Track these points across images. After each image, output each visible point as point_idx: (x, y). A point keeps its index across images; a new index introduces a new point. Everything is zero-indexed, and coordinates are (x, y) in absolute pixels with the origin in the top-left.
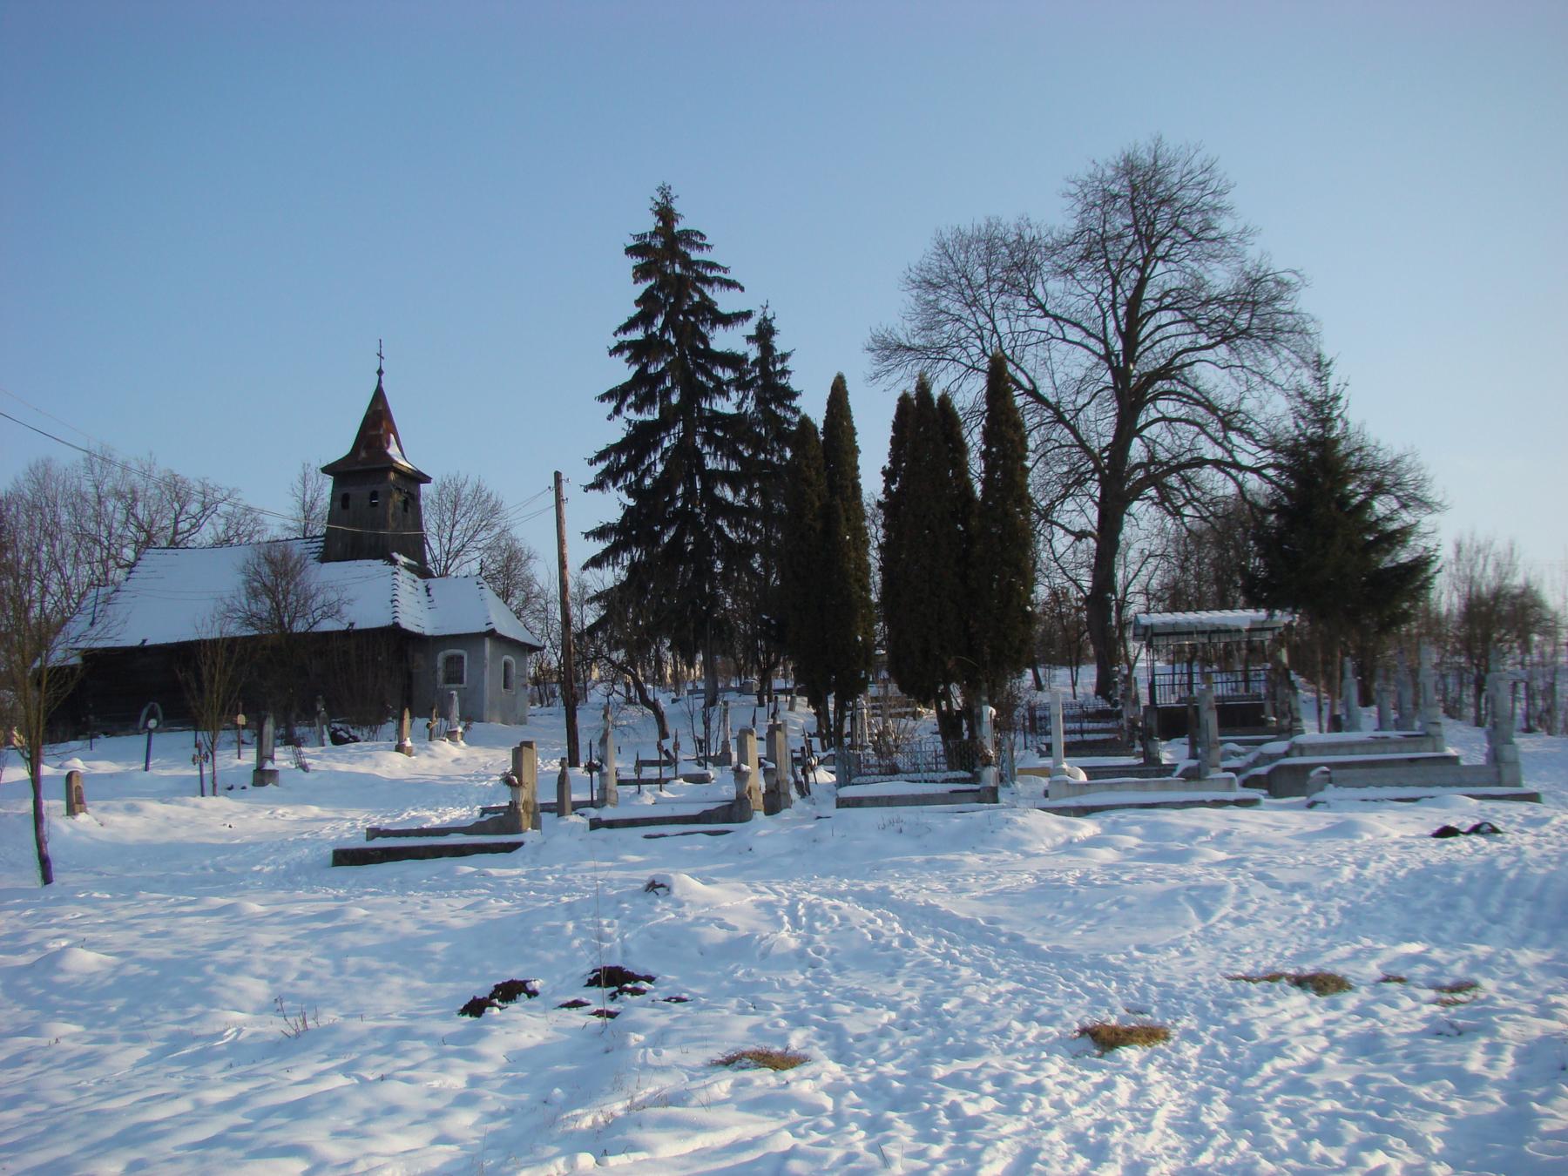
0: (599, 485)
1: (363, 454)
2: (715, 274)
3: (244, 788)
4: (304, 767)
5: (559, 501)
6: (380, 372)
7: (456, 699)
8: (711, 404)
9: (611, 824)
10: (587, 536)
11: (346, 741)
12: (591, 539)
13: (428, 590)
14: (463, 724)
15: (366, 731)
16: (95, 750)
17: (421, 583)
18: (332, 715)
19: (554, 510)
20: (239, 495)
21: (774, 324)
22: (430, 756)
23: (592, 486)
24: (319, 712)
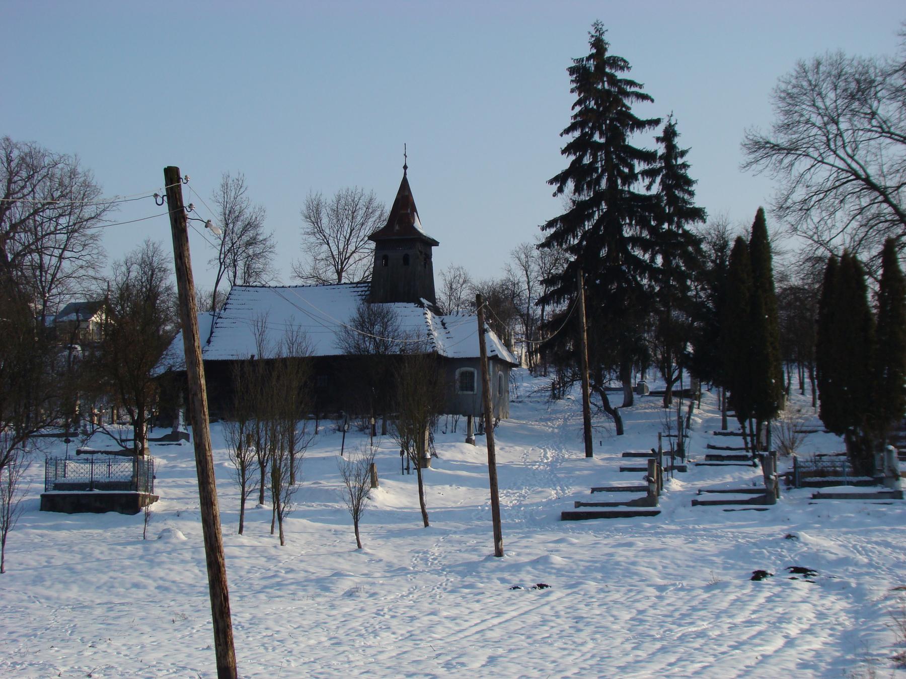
1: (397, 227)
2: (633, 89)
6: (405, 167)
8: (629, 187)
9: (703, 503)
13: (443, 324)
21: (677, 128)
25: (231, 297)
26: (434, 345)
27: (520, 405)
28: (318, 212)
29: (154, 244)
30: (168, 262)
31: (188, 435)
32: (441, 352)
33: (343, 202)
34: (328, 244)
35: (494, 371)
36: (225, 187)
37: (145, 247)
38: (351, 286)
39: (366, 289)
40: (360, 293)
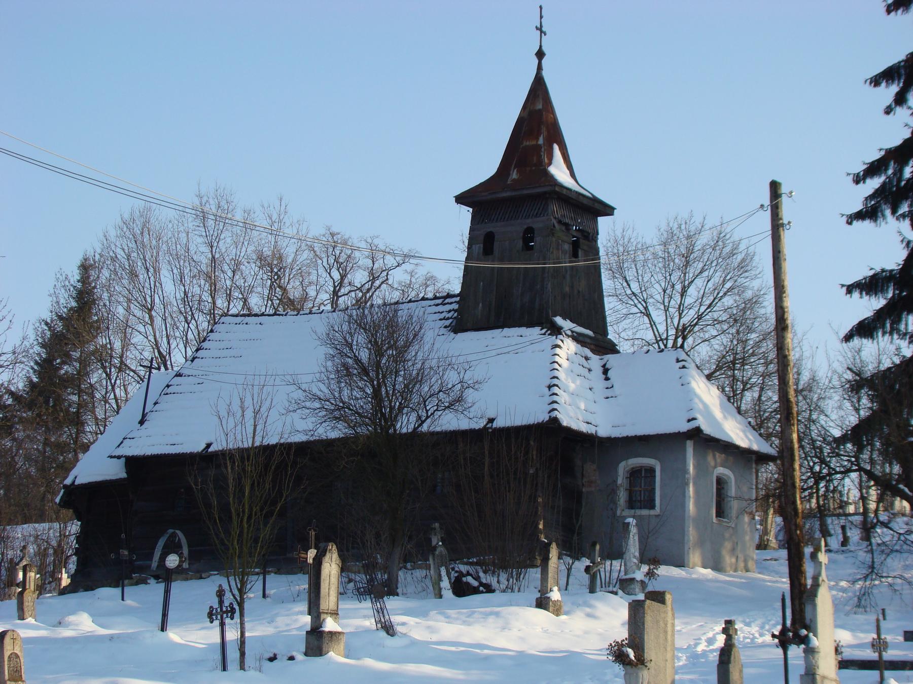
0: (869, 213)
3: (292, 658)
4: (388, 629)
5: (777, 226)
6: (540, 54)
7: (633, 530)
10: (850, 289)
11: (475, 591)
12: (856, 294)
13: (606, 371)
14: (645, 568)
15: (503, 577)
16: (129, 602)
17: (596, 361)
18: (455, 554)
19: (769, 241)
22: (589, 615)
23: (860, 216)
24: (435, 548)
26: (555, 406)
40: (442, 316)
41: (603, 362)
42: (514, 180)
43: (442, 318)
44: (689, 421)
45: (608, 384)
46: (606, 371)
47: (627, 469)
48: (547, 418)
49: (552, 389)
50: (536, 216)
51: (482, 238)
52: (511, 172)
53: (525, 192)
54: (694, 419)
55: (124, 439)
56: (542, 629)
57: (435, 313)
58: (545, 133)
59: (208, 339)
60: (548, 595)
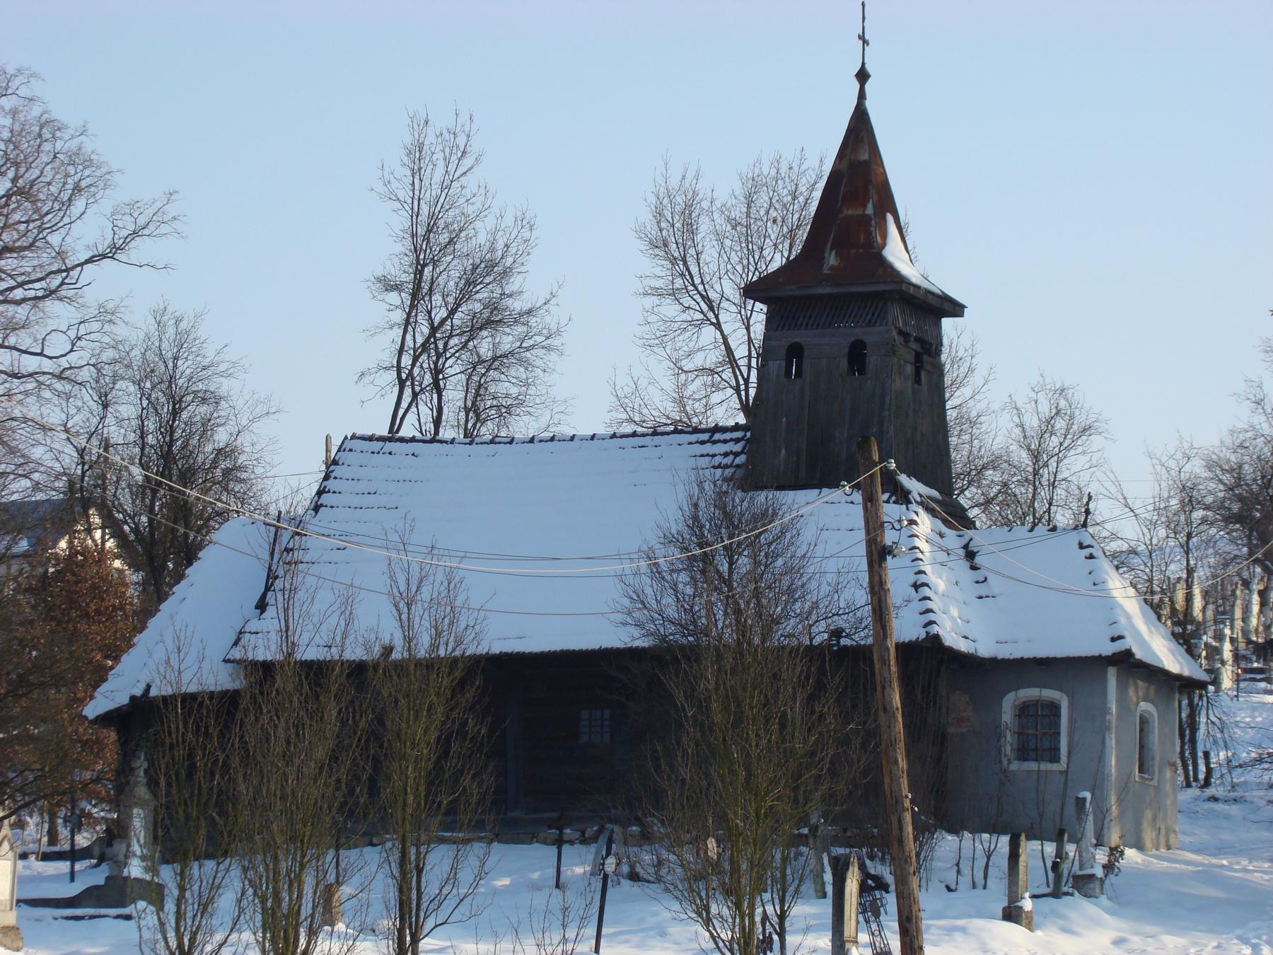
1: (832, 260)
6: (863, 76)
13: (970, 555)
20: (36, 88)
25: (338, 471)
26: (931, 617)
27: (1234, 809)
28: (690, 228)
29: (178, 321)
30: (221, 374)
31: (160, 888)
32: (952, 639)
33: (763, 199)
34: (718, 326)
35: (1122, 700)
36: (417, 156)
37: (153, 327)
38: (694, 437)
39: (738, 447)
40: (718, 460)
41: (964, 541)
42: (832, 268)
43: (717, 464)
44: (1113, 640)
45: (978, 575)
46: (970, 555)
47: (1016, 703)
48: (923, 636)
49: (920, 590)
50: (869, 324)
51: (783, 352)
52: (827, 255)
53: (854, 289)
54: (1121, 637)
55: (240, 633)
56: (1028, 951)
57: (702, 456)
58: (875, 198)
59: (333, 475)
60: (1019, 904)
